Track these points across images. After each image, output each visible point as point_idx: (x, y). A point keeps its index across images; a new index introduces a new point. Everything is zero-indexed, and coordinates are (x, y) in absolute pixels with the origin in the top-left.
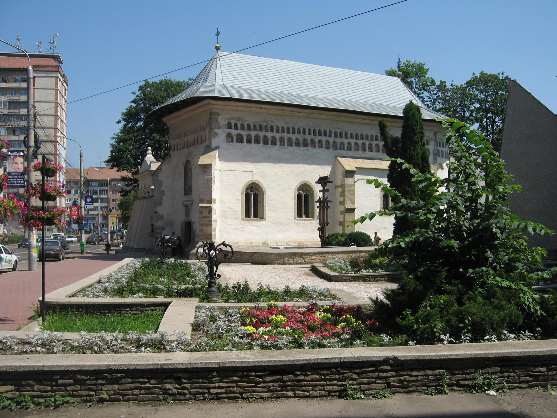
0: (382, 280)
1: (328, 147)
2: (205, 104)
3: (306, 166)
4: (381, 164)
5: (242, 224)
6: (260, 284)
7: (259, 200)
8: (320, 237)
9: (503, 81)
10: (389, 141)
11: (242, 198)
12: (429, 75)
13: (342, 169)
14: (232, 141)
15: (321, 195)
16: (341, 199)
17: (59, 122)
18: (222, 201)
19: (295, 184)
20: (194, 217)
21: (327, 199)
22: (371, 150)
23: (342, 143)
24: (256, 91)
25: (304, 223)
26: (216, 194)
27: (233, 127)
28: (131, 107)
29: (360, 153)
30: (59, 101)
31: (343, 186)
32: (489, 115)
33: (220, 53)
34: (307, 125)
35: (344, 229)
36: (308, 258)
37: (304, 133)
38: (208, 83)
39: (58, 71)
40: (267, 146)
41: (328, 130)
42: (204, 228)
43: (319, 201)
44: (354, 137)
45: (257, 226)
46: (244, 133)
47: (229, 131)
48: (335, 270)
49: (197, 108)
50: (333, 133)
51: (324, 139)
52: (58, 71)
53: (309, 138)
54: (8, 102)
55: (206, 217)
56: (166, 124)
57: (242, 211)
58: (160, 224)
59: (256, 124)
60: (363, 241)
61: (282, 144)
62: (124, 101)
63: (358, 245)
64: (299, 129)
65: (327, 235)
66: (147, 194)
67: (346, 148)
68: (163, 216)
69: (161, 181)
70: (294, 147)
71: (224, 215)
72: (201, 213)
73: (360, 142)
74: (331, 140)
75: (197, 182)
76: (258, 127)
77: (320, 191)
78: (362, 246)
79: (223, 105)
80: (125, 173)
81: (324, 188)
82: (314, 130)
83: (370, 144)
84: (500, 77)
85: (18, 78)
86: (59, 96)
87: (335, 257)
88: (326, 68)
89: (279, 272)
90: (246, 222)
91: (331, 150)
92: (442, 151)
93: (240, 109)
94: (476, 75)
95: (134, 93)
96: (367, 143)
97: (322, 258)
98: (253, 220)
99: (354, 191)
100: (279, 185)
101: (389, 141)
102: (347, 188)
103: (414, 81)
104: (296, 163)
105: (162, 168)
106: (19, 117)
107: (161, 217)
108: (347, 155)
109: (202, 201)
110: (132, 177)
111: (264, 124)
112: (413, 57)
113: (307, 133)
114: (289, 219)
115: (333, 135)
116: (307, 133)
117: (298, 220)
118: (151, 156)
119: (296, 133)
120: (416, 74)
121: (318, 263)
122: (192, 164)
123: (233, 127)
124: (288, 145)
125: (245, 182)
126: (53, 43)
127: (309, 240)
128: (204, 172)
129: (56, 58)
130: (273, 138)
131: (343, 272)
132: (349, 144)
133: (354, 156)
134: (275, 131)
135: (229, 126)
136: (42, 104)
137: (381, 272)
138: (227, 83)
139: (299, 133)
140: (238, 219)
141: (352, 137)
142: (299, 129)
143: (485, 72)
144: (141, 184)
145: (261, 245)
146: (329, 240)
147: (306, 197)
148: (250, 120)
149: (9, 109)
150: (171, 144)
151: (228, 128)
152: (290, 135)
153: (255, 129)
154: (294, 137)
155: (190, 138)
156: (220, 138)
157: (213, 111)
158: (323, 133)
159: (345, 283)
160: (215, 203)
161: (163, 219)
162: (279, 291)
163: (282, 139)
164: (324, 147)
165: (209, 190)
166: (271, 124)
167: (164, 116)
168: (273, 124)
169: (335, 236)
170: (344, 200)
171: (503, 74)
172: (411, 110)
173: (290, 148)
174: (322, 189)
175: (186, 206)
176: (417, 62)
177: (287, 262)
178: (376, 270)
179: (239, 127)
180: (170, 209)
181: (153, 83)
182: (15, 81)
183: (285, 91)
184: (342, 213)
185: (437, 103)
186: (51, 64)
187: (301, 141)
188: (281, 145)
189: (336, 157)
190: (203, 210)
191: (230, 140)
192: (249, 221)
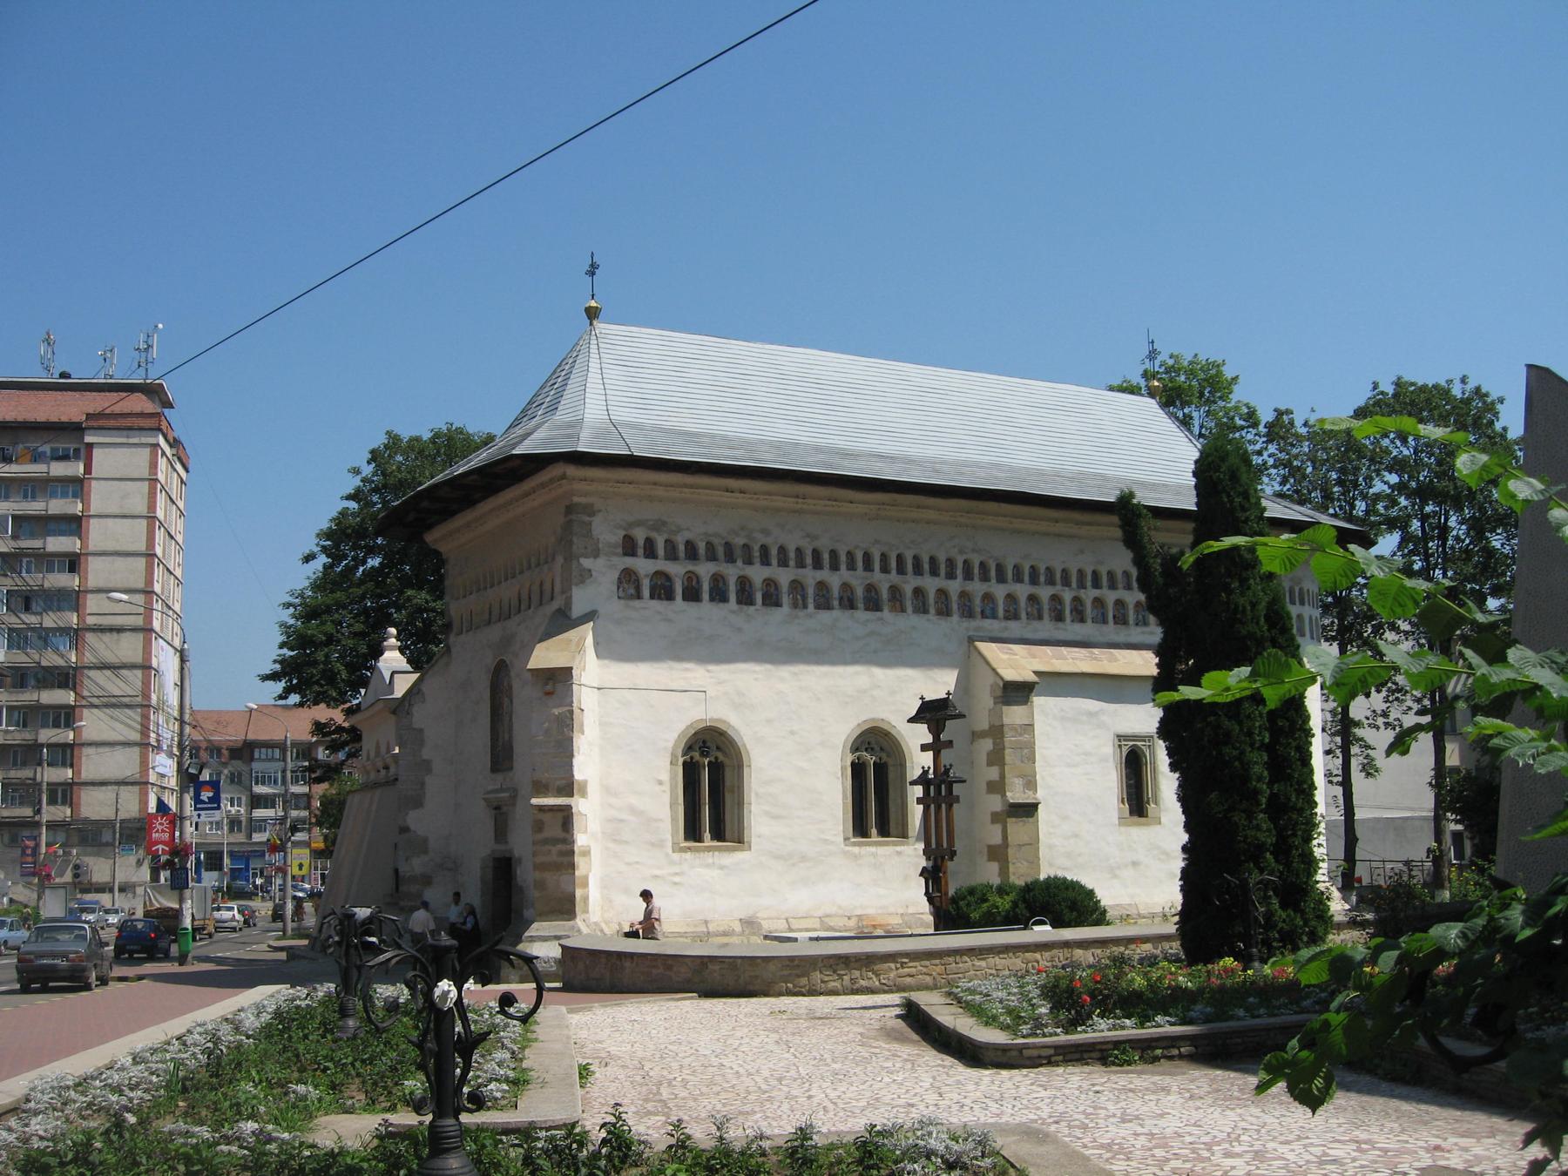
0: (1171, 1058)
1: (944, 612)
2: (552, 481)
3: (879, 673)
4: (1114, 659)
5: (672, 863)
6: (678, 1125)
7: (728, 783)
8: (930, 900)
9: (1467, 402)
10: (1156, 565)
11: (673, 778)
12: (1239, 395)
13: (991, 679)
14: (639, 596)
15: (927, 759)
16: (993, 773)
17: (158, 573)
18: (607, 790)
19: (844, 729)
20: (521, 843)
21: (947, 771)
22: (1079, 616)
23: (988, 598)
24: (714, 436)
25: (874, 855)
26: (586, 764)
27: (640, 551)
28: (344, 513)
29: (1046, 628)
30: (160, 514)
31: (997, 731)
32: (1429, 509)
33: (600, 326)
34: (877, 542)
35: (1004, 871)
36: (891, 972)
37: (868, 566)
38: (561, 416)
39: (160, 430)
40: (752, 608)
41: (942, 558)
42: (550, 877)
43: (923, 780)
44: (1026, 578)
45: (722, 868)
46: (677, 570)
47: (629, 562)
48: (991, 1021)
49: (527, 494)
50: (960, 565)
51: (931, 584)
52: (160, 430)
53: (883, 582)
54: (14, 517)
55: (555, 841)
56: (445, 556)
57: (674, 819)
58: (416, 865)
59: (716, 541)
60: (1073, 906)
61: (799, 602)
62: (327, 493)
63: (1057, 923)
64: (850, 555)
65: (951, 892)
66: (383, 772)
67: (1001, 612)
68: (425, 840)
69: (421, 731)
70: (836, 613)
71: (614, 833)
72: (539, 826)
73: (1045, 593)
74: (954, 587)
75: (527, 727)
76: (720, 551)
77: (924, 748)
78: (1068, 925)
79: (608, 481)
80: (322, 713)
81: (936, 737)
82: (900, 558)
83: (1076, 599)
84: (1457, 391)
85: (47, 448)
86: (161, 499)
87: (983, 964)
88: (929, 370)
89: (791, 1027)
90: (688, 855)
91: (955, 618)
92: (1300, 617)
93: (660, 492)
94: (1381, 388)
95: (356, 471)
96: (1067, 596)
97: (940, 969)
98: (709, 849)
99: (1031, 747)
100: (792, 733)
101: (1156, 565)
102: (1009, 738)
103: (1195, 414)
104: (845, 663)
105: (425, 688)
106: (47, 561)
107: (422, 846)
108: (1005, 635)
109: (541, 788)
110: (346, 725)
111: (739, 541)
112: (1188, 343)
113: (877, 566)
114: (826, 841)
115: (959, 572)
116: (877, 566)
117: (854, 844)
118: (397, 654)
119: (843, 567)
120: (1202, 395)
121: (927, 988)
122: (512, 674)
123: (640, 551)
124: (818, 607)
125: (683, 727)
126: (146, 350)
127: (892, 910)
128: (549, 694)
129: (153, 391)
130: (770, 583)
131: (1025, 1029)
132: (1011, 598)
133: (1029, 636)
134: (774, 562)
135: (629, 547)
136: (110, 521)
137: (1164, 1026)
138: (620, 415)
139: (851, 566)
140: (658, 845)
141: (1018, 578)
142: (850, 555)
143: (1407, 378)
144: (368, 744)
145: (738, 927)
146: (958, 908)
147: (881, 769)
148: (694, 527)
149: (15, 537)
150: (453, 613)
151: (625, 554)
152: (824, 574)
153: (712, 556)
154: (835, 581)
155: (507, 591)
156: (598, 584)
157: (576, 499)
158: (926, 567)
159: (1032, 1074)
160: (584, 794)
161: (426, 852)
162: (766, 1144)
163: (797, 586)
164: (932, 611)
165: (565, 751)
166: (762, 539)
167: (430, 527)
168: (768, 541)
169: (977, 894)
170: (1003, 776)
171: (1464, 380)
172: (1223, 459)
173: (825, 616)
174: (929, 739)
175: (497, 808)
176: (1202, 358)
177: (820, 987)
178: (1144, 1020)
179: (661, 552)
180: (448, 818)
181: (412, 440)
182: (36, 458)
183: (804, 440)
184: (996, 818)
185: (1265, 479)
186: (138, 409)
187: (860, 592)
188: (795, 606)
189: (971, 640)
190: (546, 817)
191: (632, 591)
192: (697, 850)
